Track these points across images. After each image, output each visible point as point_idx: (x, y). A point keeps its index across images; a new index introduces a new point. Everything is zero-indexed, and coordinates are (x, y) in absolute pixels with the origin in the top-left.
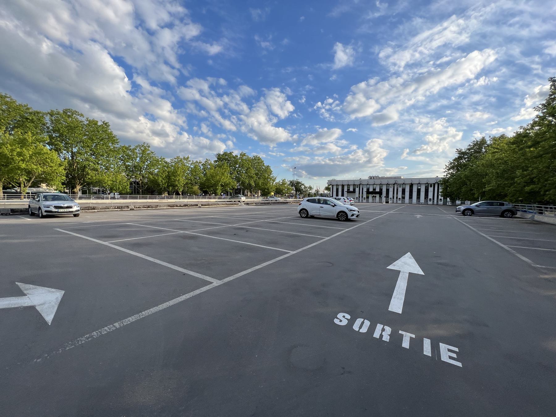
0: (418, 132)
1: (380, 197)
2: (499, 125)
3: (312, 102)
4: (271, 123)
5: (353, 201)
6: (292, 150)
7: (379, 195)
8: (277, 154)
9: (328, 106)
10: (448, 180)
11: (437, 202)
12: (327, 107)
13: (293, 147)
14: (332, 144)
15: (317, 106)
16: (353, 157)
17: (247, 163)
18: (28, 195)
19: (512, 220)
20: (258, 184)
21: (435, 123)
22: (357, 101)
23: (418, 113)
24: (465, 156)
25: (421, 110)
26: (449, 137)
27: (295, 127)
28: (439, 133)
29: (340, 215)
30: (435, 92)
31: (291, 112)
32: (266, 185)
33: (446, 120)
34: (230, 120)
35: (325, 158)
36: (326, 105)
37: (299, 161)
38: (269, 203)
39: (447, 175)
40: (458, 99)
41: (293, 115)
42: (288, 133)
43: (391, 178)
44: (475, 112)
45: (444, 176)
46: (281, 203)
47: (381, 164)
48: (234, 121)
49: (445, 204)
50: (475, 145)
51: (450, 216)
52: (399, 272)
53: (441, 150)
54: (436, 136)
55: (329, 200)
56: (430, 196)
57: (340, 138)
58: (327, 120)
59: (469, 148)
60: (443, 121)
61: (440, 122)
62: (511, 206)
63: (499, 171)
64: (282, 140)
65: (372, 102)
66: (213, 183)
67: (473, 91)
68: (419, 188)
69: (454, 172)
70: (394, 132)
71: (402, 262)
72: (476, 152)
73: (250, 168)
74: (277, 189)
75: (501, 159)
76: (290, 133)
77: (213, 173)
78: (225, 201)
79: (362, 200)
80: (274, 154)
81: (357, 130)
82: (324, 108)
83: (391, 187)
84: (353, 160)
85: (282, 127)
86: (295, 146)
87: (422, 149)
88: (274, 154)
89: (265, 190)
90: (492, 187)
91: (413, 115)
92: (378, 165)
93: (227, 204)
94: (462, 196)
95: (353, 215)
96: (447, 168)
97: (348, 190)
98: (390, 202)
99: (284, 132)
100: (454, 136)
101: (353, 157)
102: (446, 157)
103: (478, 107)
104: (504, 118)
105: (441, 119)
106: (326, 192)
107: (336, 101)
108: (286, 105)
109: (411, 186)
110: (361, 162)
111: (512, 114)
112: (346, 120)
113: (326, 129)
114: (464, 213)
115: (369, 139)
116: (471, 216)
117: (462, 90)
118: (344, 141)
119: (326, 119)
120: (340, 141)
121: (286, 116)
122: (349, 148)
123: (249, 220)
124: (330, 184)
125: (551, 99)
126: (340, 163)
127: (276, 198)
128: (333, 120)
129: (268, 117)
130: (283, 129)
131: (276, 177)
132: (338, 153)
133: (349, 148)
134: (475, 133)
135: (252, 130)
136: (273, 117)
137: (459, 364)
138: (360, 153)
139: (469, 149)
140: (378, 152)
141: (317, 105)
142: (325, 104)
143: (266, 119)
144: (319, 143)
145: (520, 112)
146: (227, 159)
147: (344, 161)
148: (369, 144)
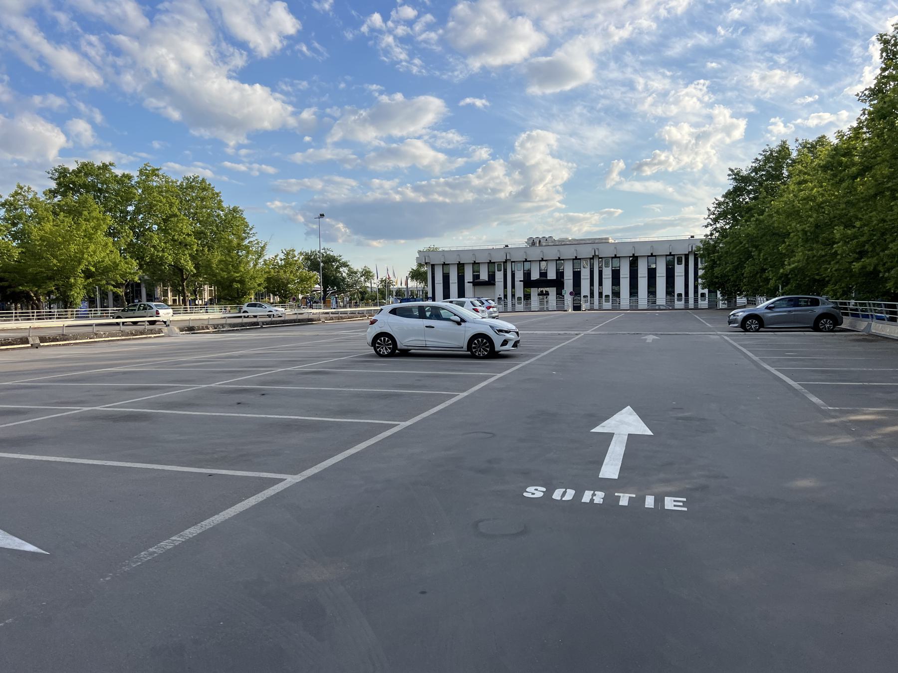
0: (644, 116)
1: (559, 294)
2: (822, 104)
3: (353, 13)
4: (225, 69)
5: (495, 309)
6: (298, 157)
7: (555, 288)
8: (251, 169)
9: (402, 27)
10: (714, 246)
11: (696, 301)
12: (401, 30)
13: (304, 147)
14: (419, 143)
15: (369, 26)
16: (482, 181)
17: (164, 201)
18: (96, 313)
19: (833, 336)
20: (208, 265)
21: (683, 93)
22: (484, 19)
23: (642, 63)
24: (749, 186)
25: (649, 58)
26: (716, 130)
27: (304, 85)
28: (694, 119)
29: (475, 344)
30: (680, 11)
31: (289, 37)
32: (236, 268)
33: (707, 88)
34: (76, 48)
35: (402, 184)
36: (397, 22)
37: (322, 192)
38: (256, 324)
39: (712, 234)
40: (732, 33)
41: (297, 47)
42: (284, 102)
43: (583, 242)
44: (771, 68)
45: (706, 236)
46: (284, 322)
47: (557, 202)
48: (92, 52)
49: (713, 306)
50: (767, 159)
51: (717, 335)
52: (611, 435)
53: (700, 166)
54: (686, 128)
55: (445, 307)
56: (679, 287)
57: (444, 124)
58: (401, 70)
59: (756, 167)
60: (701, 90)
61: (694, 91)
62: (831, 306)
63: (809, 227)
64: (267, 125)
65: (525, 26)
66: (55, 265)
67: (764, 15)
68: (653, 266)
69: (728, 227)
70: (585, 111)
71: (616, 421)
72: (770, 176)
73: (175, 216)
74: (268, 280)
75: (811, 200)
76: (290, 103)
77: (51, 233)
78: (91, 325)
79: (513, 305)
80: (242, 168)
81: (488, 104)
82: (390, 32)
83: (584, 267)
84: (480, 191)
85: (263, 83)
86: (308, 146)
87: (656, 161)
88: (242, 168)
89: (231, 286)
90: (796, 264)
91: (629, 70)
92: (547, 203)
93: (123, 333)
94: (745, 285)
95: (505, 343)
96: (711, 216)
97: (476, 277)
98: (584, 307)
99: (272, 99)
100: (728, 130)
101: (482, 181)
102: (714, 184)
103: (776, 57)
104: (832, 88)
105: (696, 83)
106: (413, 284)
107: (426, 13)
108: (271, 12)
109: (634, 262)
110: (502, 195)
111: (848, 80)
112: (456, 73)
113: (399, 97)
114: (744, 325)
115: (523, 130)
116: (757, 331)
117: (740, 12)
118: (454, 133)
119: (398, 66)
120: (444, 134)
121: (276, 47)
122: (468, 156)
123: (239, 371)
124: (426, 263)
125: (884, 77)
126: (447, 200)
127: (268, 309)
128: (420, 72)
129: (215, 48)
130: (268, 89)
131: (266, 244)
132: (437, 169)
133: (468, 156)
134: (774, 124)
135: (160, 87)
136: (231, 49)
137: (685, 509)
138: (499, 169)
139: (756, 170)
140: (545, 167)
141: (370, 20)
142: (393, 22)
143: (208, 54)
144: (381, 139)
145: (863, 76)
146: (94, 186)
147: (457, 192)
148: (522, 145)
